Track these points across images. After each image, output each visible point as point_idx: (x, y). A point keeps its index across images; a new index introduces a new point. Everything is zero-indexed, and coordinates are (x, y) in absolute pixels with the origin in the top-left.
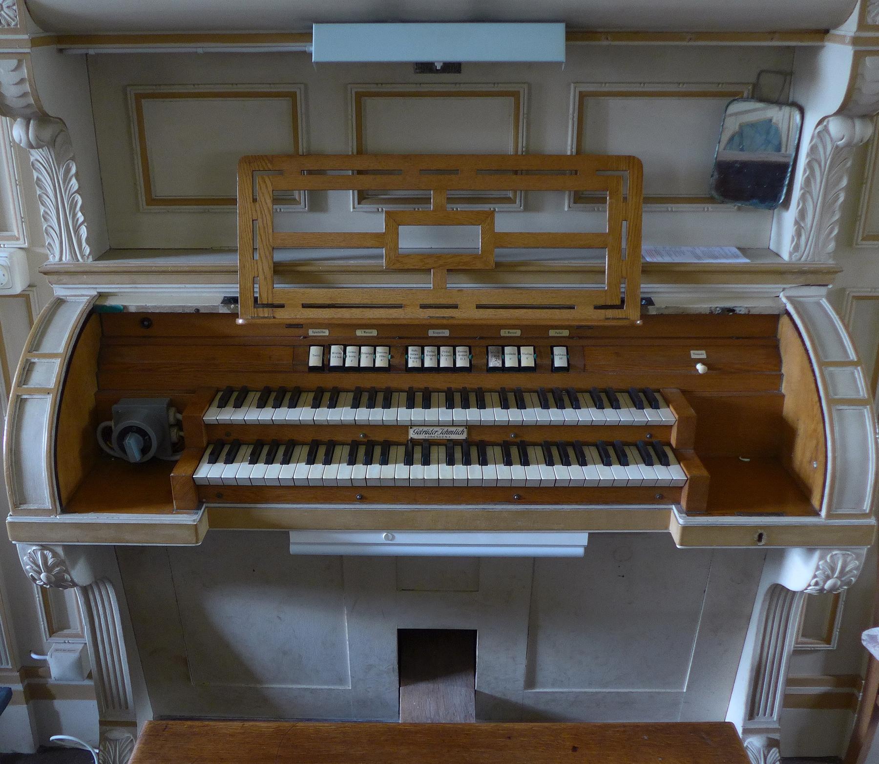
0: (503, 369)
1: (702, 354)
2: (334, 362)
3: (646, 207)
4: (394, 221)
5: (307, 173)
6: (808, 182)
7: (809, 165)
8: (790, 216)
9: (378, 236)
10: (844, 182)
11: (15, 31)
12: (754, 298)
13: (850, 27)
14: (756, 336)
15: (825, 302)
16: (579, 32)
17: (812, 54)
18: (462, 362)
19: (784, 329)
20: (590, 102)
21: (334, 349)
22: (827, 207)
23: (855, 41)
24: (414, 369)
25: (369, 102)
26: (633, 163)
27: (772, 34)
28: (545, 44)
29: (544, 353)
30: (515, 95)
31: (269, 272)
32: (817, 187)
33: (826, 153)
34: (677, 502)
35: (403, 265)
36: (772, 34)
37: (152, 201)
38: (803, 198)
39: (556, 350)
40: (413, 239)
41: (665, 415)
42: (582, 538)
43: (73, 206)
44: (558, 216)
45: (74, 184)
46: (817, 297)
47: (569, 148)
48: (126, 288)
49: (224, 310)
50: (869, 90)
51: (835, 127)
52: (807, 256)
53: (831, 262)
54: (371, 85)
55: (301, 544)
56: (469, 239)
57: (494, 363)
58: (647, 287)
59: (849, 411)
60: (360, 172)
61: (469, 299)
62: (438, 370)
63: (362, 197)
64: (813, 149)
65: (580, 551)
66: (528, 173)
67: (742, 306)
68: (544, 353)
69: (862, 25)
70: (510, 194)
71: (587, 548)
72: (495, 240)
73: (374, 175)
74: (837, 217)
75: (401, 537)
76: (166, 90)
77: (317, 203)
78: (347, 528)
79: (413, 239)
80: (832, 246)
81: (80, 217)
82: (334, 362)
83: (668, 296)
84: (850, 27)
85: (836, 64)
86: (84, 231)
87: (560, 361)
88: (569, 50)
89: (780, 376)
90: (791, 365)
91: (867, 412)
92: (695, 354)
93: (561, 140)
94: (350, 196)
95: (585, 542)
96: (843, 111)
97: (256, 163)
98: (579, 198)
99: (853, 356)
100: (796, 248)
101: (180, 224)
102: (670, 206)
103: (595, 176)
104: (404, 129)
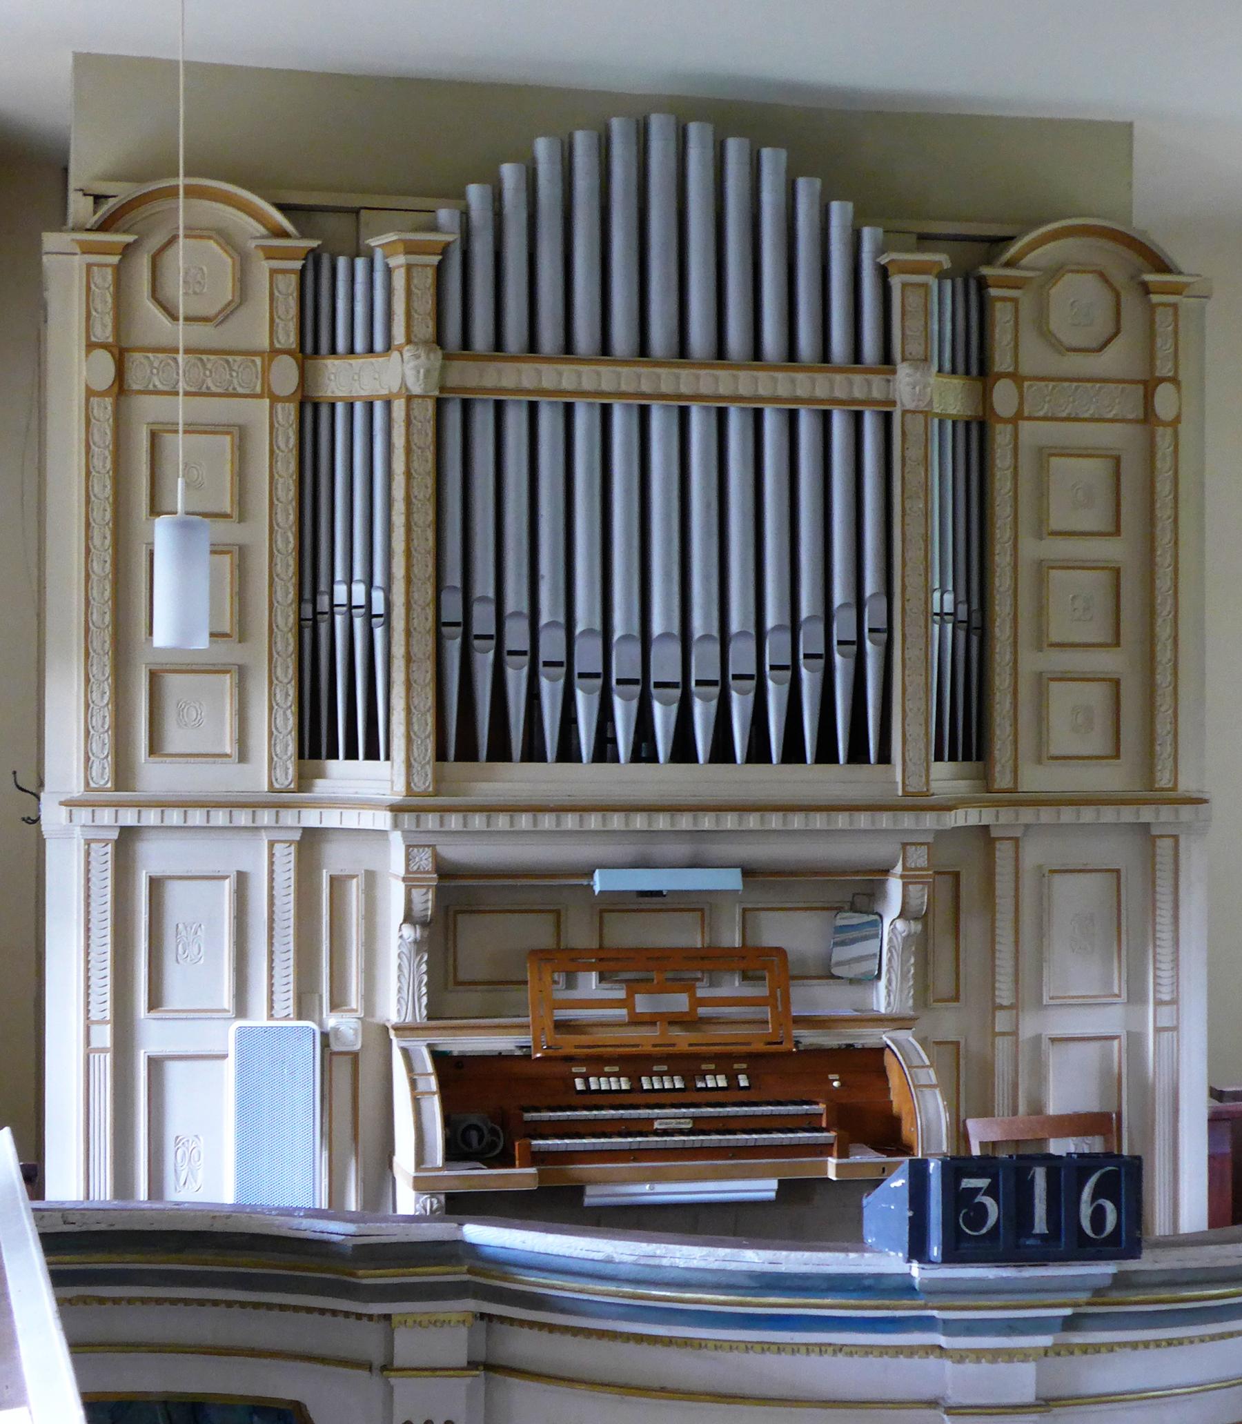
0: (707, 1089)
1: (837, 1077)
2: (593, 1087)
3: (792, 982)
4: (631, 994)
5: (568, 961)
6: (890, 960)
7: (890, 950)
8: (882, 983)
9: (621, 1000)
10: (912, 960)
11: (428, 872)
12: (869, 1037)
13: (899, 869)
14: (871, 1062)
15: (911, 1039)
16: (749, 873)
17: (883, 884)
18: (679, 1085)
19: (888, 1059)
20: (748, 914)
21: (591, 1079)
22: (904, 976)
23: (902, 877)
24: (647, 1090)
25: (606, 915)
26: (780, 952)
27: (857, 873)
28: (731, 880)
29: (732, 1078)
30: (702, 910)
31: (552, 1026)
32: (896, 963)
33: (898, 942)
34: (831, 1155)
35: (636, 1021)
36: (857, 873)
37: (458, 983)
38: (888, 971)
39: (740, 1077)
40: (643, 1004)
41: (821, 1108)
42: (773, 1184)
43: (420, 982)
44: (733, 987)
45: (424, 967)
46: (906, 1036)
47: (737, 943)
48: (448, 1039)
49: (518, 1053)
50: (914, 903)
51: (900, 925)
52: (896, 1009)
53: (912, 1013)
54: (617, 903)
55: (594, 1196)
56: (679, 1002)
57: (700, 1085)
58: (796, 1032)
59: (927, 1091)
60: (601, 960)
61: (682, 1040)
62: (663, 1090)
63: (602, 979)
64: (890, 940)
65: (772, 1195)
66: (713, 960)
67: (859, 1043)
68: (732, 1078)
69: (904, 868)
70: (699, 975)
71: (778, 1192)
72: (698, 1002)
73: (609, 963)
74: (911, 983)
75: (659, 1188)
76: (482, 908)
77: (571, 984)
78: (624, 1182)
79: (643, 1004)
80: (911, 1002)
81: (424, 990)
82: (593, 1087)
83: (810, 1038)
84: (899, 869)
85: (895, 887)
86: (425, 1000)
87: (743, 1081)
88: (745, 884)
89: (888, 1089)
90: (894, 1080)
91: (937, 1091)
92: (831, 1077)
93: (733, 939)
94: (594, 976)
95: (776, 1187)
96: (902, 915)
97: (541, 956)
98: (745, 977)
99: (928, 1063)
100: (889, 1004)
101: (474, 998)
102: (805, 981)
103: (758, 962)
104: (630, 933)
